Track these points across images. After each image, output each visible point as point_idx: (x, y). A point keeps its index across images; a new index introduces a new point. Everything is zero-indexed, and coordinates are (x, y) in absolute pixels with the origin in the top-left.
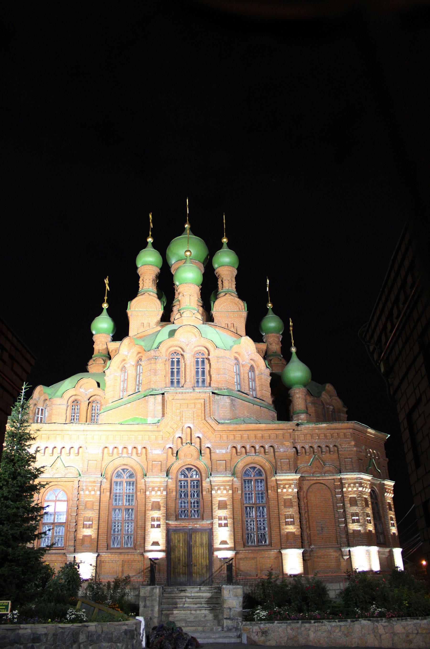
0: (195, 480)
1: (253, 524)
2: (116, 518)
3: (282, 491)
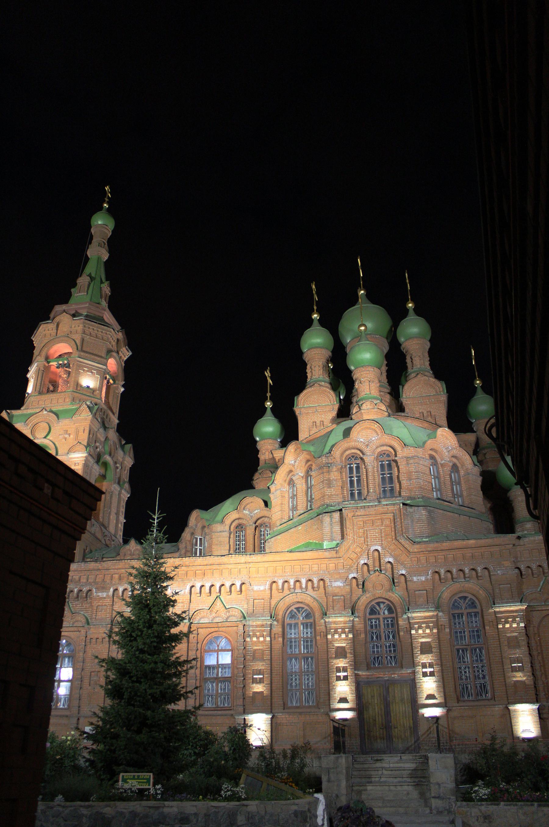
0: (389, 618)
1: (469, 672)
2: (292, 669)
3: (504, 627)
